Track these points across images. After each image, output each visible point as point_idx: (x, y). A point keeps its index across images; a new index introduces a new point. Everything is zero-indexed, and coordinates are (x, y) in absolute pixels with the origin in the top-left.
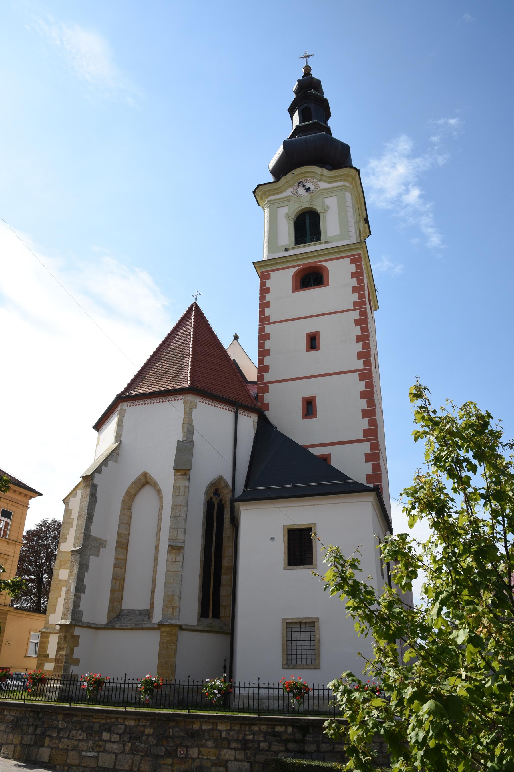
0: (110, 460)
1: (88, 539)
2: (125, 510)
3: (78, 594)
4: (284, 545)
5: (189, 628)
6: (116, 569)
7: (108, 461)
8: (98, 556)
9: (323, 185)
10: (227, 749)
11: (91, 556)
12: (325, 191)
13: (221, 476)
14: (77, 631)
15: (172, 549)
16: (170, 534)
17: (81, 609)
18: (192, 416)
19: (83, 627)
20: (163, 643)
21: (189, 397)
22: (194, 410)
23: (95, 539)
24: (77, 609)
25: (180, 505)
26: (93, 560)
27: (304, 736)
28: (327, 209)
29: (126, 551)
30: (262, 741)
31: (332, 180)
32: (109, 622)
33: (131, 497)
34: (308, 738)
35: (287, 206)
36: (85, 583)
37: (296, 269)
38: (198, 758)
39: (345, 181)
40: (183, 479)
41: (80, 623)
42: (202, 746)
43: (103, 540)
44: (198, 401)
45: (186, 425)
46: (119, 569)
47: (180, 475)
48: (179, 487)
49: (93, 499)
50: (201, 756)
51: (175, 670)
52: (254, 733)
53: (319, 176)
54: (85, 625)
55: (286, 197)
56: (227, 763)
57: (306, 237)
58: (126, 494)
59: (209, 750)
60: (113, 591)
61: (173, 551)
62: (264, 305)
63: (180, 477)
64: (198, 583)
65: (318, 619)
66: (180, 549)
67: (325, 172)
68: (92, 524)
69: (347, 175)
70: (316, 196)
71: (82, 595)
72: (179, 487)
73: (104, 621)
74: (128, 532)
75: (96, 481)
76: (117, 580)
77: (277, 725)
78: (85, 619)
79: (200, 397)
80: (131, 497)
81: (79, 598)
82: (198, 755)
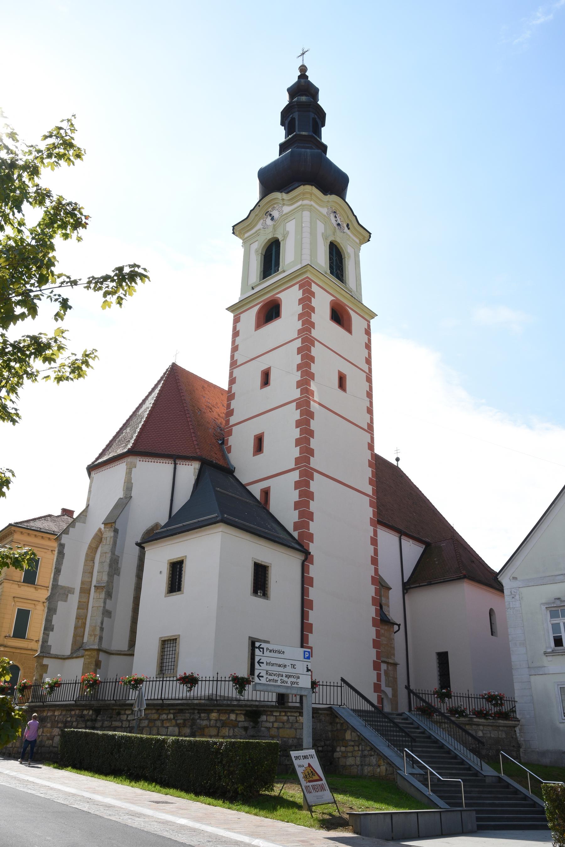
0: (77, 522)
1: (56, 588)
2: (88, 561)
3: (46, 632)
4: (167, 577)
5: (119, 652)
6: (79, 610)
7: (75, 523)
8: (66, 601)
9: (286, 209)
10: (56, 728)
11: (59, 602)
12: (286, 216)
13: (158, 523)
14: (46, 661)
15: (97, 589)
16: (97, 577)
17: (49, 643)
18: (131, 475)
19: (51, 657)
20: (86, 663)
21: (130, 459)
22: (133, 469)
23: (63, 588)
24: (45, 644)
25: (106, 553)
26: (61, 605)
27: (97, 716)
28: (287, 235)
29: (88, 595)
30: (75, 721)
31: (292, 201)
32: (72, 653)
33: (93, 550)
34: (98, 718)
35: (257, 240)
36: (53, 624)
37: (258, 307)
38: (42, 735)
39: (303, 199)
40: (109, 530)
41: (47, 655)
42: (45, 727)
43: (71, 588)
44: (138, 461)
45: (126, 483)
46: (81, 610)
47: (108, 528)
48: (107, 538)
49: (61, 556)
50: (43, 734)
51: (352, 726)
52: (71, 716)
53: (281, 201)
54: (53, 656)
55: (256, 232)
56: (54, 737)
57: (272, 269)
58: (89, 548)
59: (48, 729)
60: (76, 628)
61: (98, 591)
62: (235, 349)
63: (108, 529)
64: (131, 615)
65: (179, 635)
66: (102, 588)
67: (284, 196)
68: (60, 576)
69: (304, 194)
70: (279, 222)
71: (51, 633)
72: (107, 538)
73: (68, 652)
74: (90, 579)
75: (63, 541)
76: (79, 619)
77: (84, 710)
78: (53, 651)
79: (140, 457)
80: (93, 550)
81: (48, 635)
82: (42, 733)
